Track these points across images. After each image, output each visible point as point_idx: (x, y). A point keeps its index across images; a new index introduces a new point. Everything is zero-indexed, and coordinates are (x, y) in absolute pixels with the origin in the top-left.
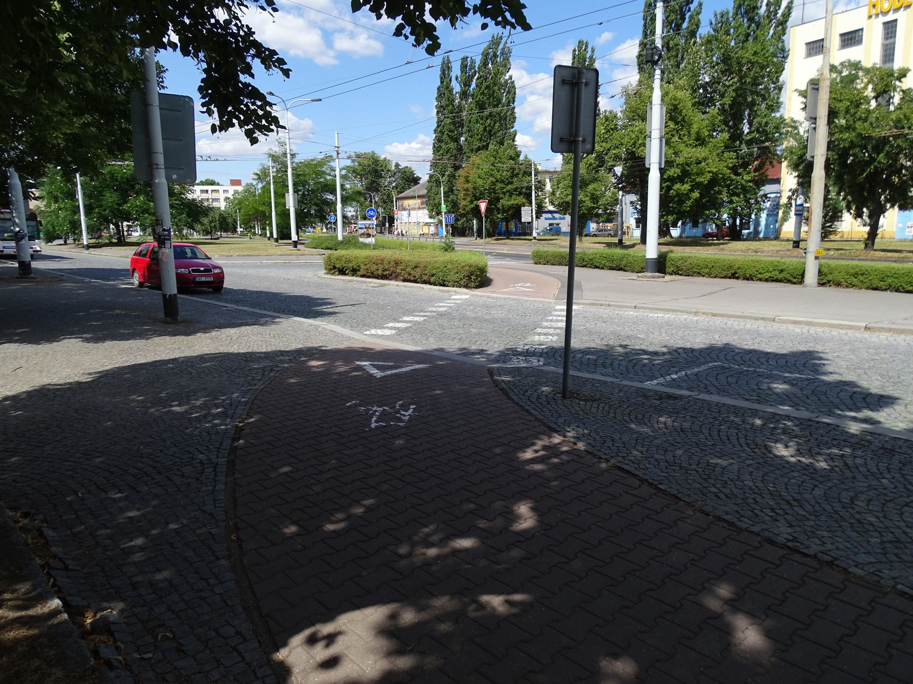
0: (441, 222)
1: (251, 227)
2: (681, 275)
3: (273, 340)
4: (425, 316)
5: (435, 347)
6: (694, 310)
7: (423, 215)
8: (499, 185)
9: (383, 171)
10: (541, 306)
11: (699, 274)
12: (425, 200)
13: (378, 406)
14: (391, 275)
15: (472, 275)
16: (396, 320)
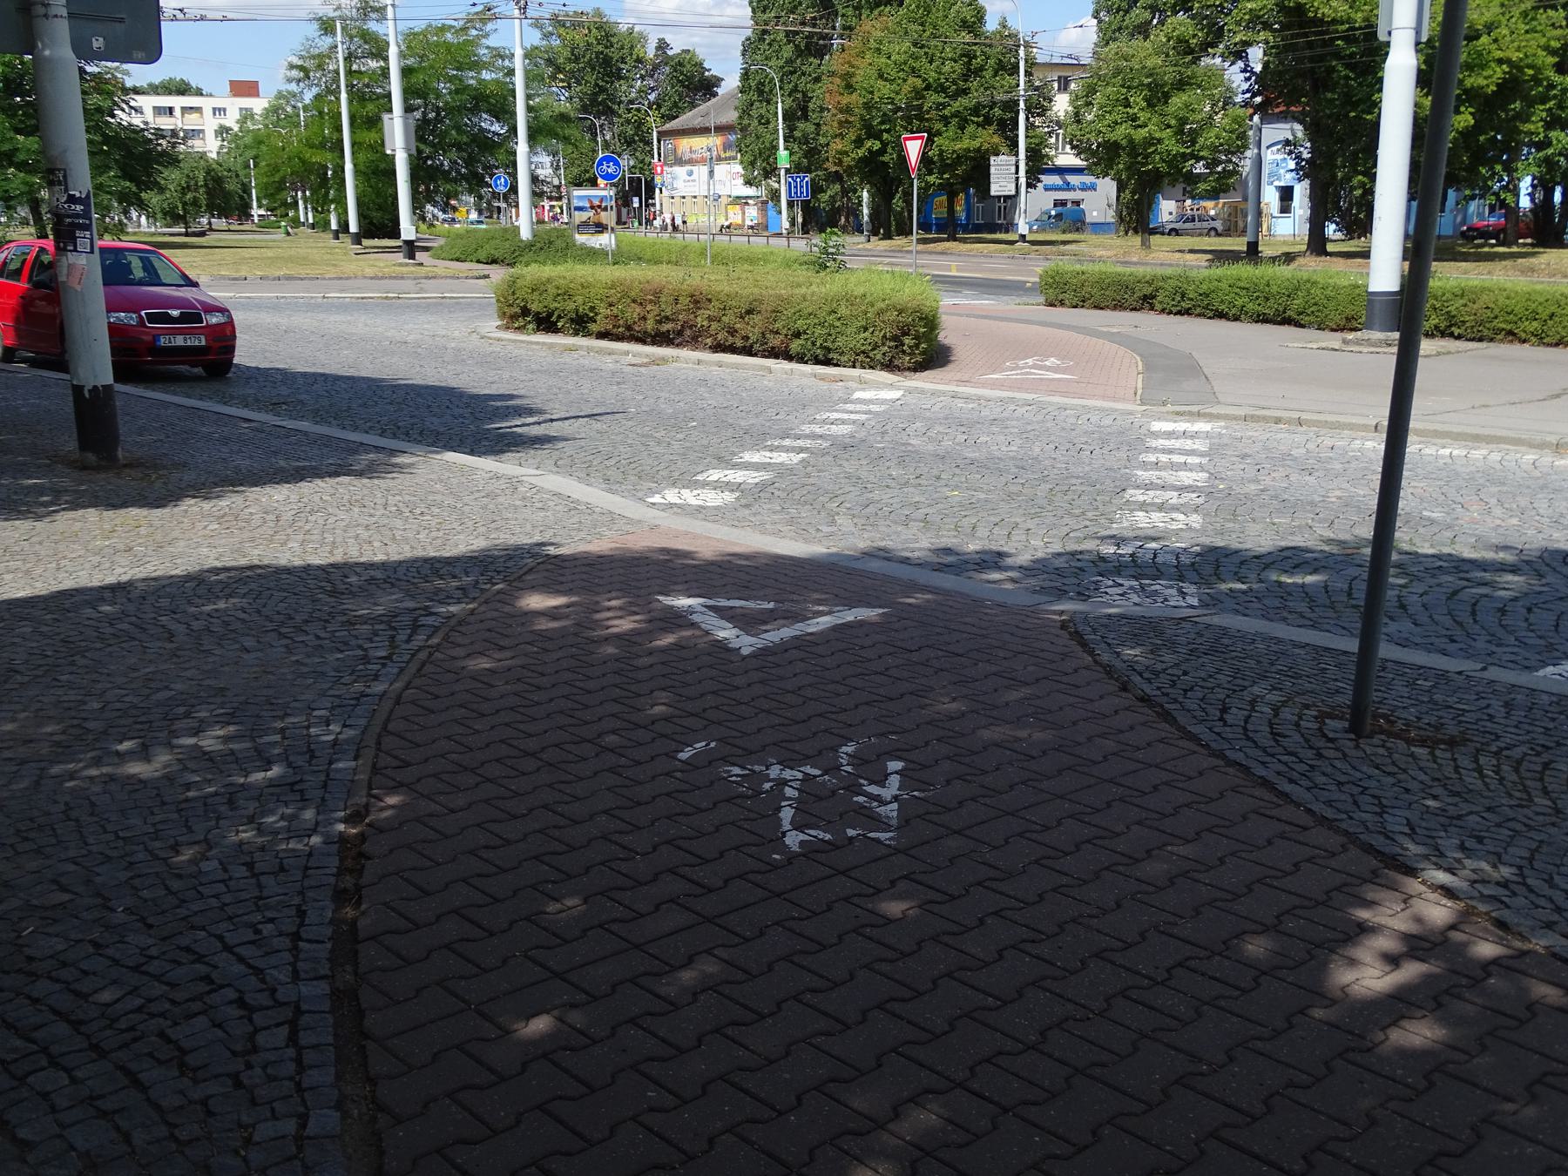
0: (775, 195)
1: (285, 204)
2: (1459, 337)
3: (398, 523)
4: (801, 450)
5: (862, 544)
6: (1553, 439)
7: (731, 178)
8: (933, 98)
9: (623, 61)
10: (1107, 421)
11: (1512, 336)
12: (732, 138)
13: (786, 764)
14: (680, 333)
15: (905, 334)
16: (723, 461)
